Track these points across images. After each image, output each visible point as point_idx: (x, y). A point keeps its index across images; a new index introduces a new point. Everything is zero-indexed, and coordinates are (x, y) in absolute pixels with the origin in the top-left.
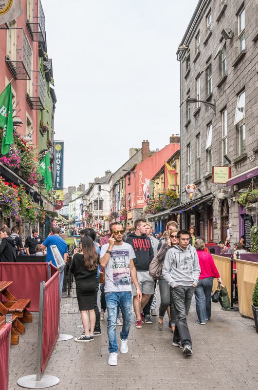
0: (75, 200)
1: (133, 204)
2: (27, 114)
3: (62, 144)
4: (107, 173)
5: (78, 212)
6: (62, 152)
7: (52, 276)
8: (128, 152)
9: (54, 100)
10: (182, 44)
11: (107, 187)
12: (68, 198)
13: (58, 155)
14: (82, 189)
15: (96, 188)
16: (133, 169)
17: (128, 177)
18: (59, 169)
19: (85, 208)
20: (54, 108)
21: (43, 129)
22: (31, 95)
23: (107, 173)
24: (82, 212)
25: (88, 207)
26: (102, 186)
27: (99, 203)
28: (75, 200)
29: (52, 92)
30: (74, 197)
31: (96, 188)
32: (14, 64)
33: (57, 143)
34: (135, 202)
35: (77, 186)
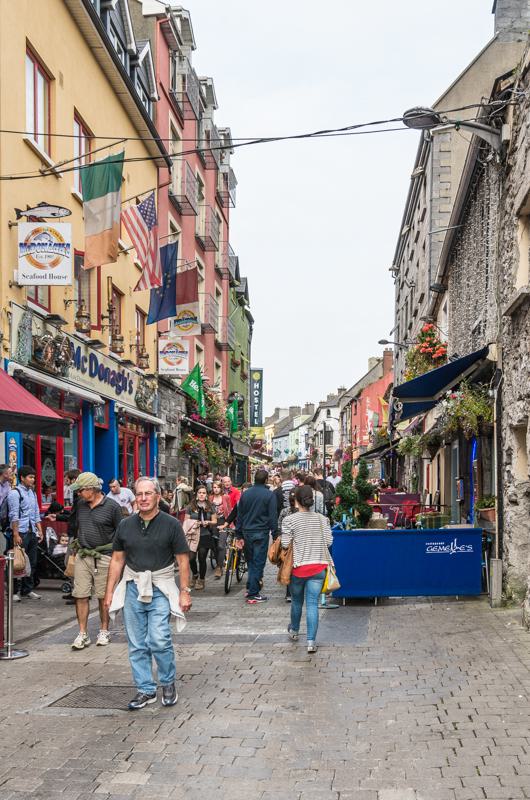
0: (298, 428)
1: (358, 440)
2: (216, 284)
3: (261, 372)
4: (340, 390)
5: (302, 445)
6: (260, 381)
7: (147, 56)
8: (367, 363)
9: (251, 320)
10: (416, 166)
11: (336, 412)
12: (288, 424)
13: (256, 386)
14: (310, 411)
15: (323, 412)
16: (359, 395)
17: (354, 404)
18: (257, 401)
19: (310, 441)
20: (251, 330)
21: (279, 624)
22: (220, 266)
23: (340, 390)
24: (308, 445)
25: (314, 440)
26: (331, 410)
27: (327, 436)
28: (298, 428)
29: (248, 315)
30: (297, 422)
31: (323, 412)
32: (203, 239)
33: (255, 371)
34: (361, 438)
35: (303, 407)
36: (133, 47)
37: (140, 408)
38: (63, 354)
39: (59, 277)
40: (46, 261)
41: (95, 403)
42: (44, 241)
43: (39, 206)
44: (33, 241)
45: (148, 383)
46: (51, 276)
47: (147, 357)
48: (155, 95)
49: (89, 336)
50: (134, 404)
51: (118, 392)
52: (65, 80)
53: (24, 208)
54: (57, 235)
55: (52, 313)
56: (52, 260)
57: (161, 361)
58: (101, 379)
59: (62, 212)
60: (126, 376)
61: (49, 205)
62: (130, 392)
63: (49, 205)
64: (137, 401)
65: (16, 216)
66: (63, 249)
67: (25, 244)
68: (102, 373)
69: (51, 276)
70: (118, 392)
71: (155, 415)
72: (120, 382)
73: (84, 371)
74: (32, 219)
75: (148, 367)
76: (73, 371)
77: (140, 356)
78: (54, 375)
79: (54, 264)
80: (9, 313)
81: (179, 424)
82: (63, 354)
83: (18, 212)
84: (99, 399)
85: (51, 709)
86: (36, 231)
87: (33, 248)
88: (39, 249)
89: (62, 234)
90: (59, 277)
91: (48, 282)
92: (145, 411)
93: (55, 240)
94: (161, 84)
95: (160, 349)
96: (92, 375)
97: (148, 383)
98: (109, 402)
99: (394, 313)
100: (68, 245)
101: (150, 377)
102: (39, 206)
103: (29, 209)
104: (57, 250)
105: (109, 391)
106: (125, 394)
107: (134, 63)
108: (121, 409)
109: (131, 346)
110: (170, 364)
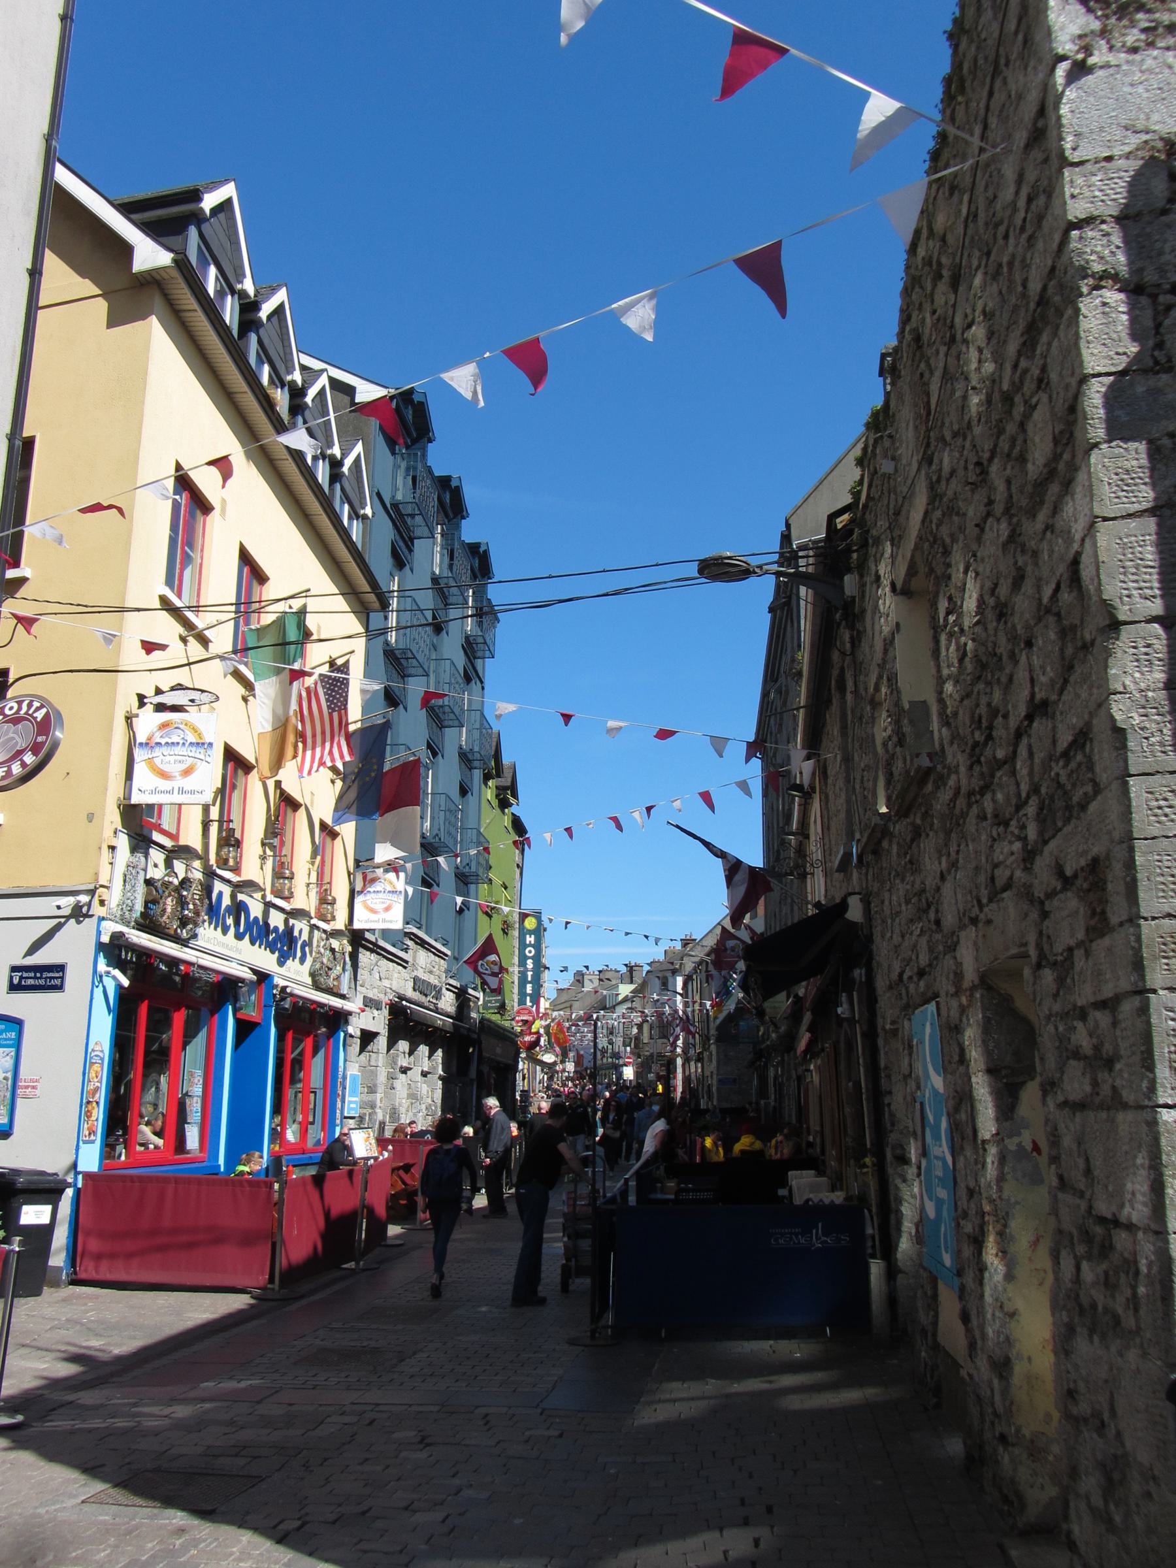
7: (357, 460)
36: (248, 286)
37: (317, 986)
38: (191, 906)
39: (192, 792)
40: (174, 769)
41: (242, 980)
42: (175, 739)
43: (173, 689)
44: (158, 740)
45: (335, 944)
46: (181, 791)
47: (333, 902)
48: (368, 511)
49: (239, 874)
50: (309, 981)
51: (281, 963)
52: (228, 508)
53: (149, 692)
54: (195, 730)
55: (182, 842)
56: (183, 767)
57: (140, 769)
58: (253, 943)
59: (205, 697)
60: (296, 933)
61: (187, 688)
62: (302, 961)
63: (187, 688)
64: (313, 975)
65: (137, 704)
66: (203, 751)
67: (147, 744)
68: (260, 933)
69: (181, 791)
70: (281, 963)
71: (343, 997)
72: (286, 945)
73: (225, 931)
74: (160, 708)
75: (334, 918)
76: (208, 935)
77: (278, 874)
78: (176, 939)
79: (387, 909)
80: (113, 848)
81: (385, 1012)
82: (191, 906)
83: (141, 699)
84: (248, 975)
85: (86, 1508)
86: (164, 726)
87: (157, 749)
88: (165, 750)
89: (201, 727)
90: (192, 792)
91: (177, 798)
92: (329, 991)
93: (191, 738)
94: (379, 495)
95: (141, 738)
96: (239, 937)
97: (335, 944)
98: (263, 977)
99: (896, 283)
100: (210, 744)
101: (335, 934)
102: (173, 689)
103: (159, 692)
104: (194, 752)
105: (266, 960)
106: (292, 965)
107: (297, 401)
108: (284, 988)
109: (308, 885)
110: (164, 775)
